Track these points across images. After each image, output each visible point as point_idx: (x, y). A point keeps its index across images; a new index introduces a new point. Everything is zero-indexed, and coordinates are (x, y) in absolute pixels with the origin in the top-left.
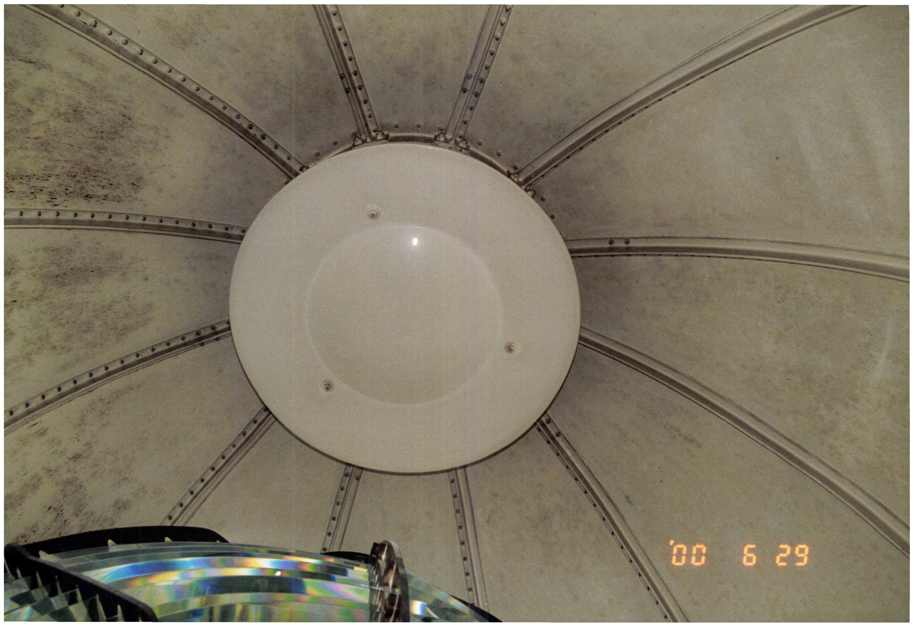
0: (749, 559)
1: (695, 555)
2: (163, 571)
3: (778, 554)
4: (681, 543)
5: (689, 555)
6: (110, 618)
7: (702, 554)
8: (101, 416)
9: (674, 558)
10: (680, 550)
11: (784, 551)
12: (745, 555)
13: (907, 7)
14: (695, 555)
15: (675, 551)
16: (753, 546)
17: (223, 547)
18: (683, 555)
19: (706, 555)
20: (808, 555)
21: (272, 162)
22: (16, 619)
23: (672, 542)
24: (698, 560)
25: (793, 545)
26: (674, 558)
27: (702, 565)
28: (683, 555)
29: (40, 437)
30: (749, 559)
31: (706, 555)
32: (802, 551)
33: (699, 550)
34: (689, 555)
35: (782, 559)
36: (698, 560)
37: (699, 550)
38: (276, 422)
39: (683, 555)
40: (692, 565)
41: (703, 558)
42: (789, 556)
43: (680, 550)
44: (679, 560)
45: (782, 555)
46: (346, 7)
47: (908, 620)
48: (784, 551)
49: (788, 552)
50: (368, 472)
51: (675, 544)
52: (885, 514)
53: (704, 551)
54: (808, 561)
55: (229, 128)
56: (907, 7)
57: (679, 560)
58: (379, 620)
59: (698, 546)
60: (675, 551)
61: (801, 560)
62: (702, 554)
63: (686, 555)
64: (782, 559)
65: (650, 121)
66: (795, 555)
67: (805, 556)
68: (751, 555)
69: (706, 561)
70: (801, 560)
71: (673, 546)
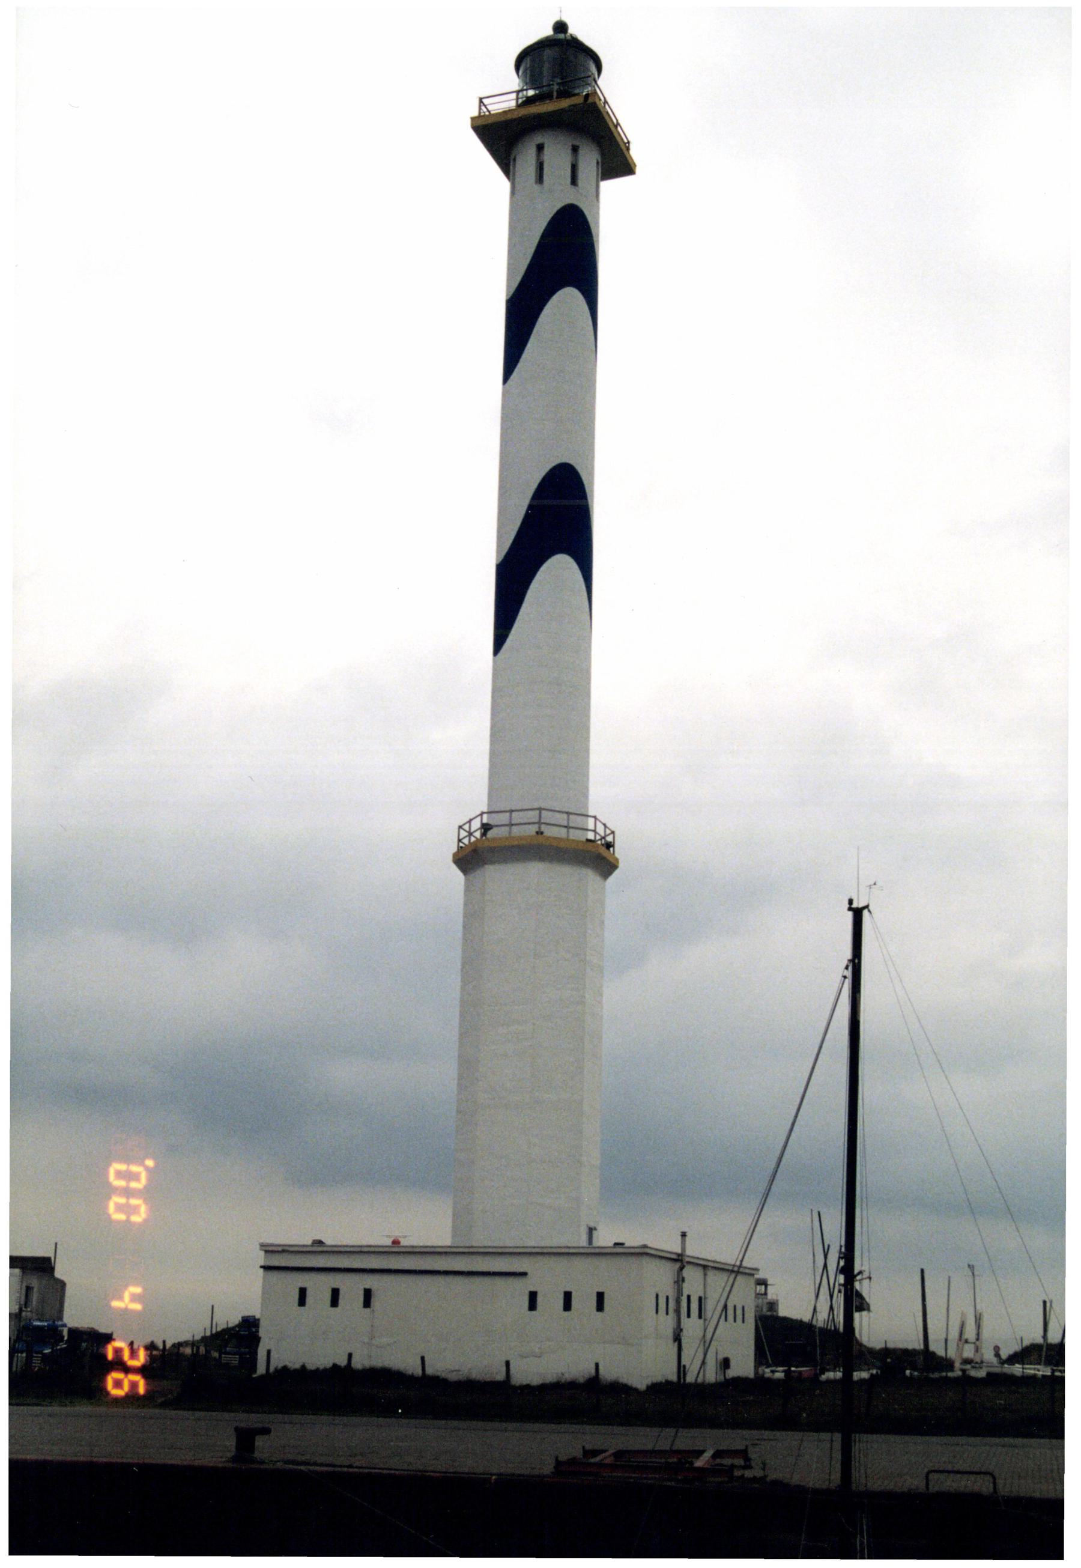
0: (118, 1384)
1: (127, 1202)
4: (148, 1179)
5: (128, 1192)
6: (13, 1317)
9: (122, 1167)
10: (136, 1177)
12: (126, 1376)
14: (127, 1202)
15: (134, 1168)
17: (293, 1464)
20: (126, 1309)
21: (663, 1251)
22: (12, 1266)
23: (150, 1163)
24: (119, 1208)
27: (109, 1216)
29: (558, 100)
33: (135, 1210)
34: (128, 1192)
36: (119, 1208)
37: (135, 1210)
41: (121, 1217)
43: (136, 1177)
44: (119, 1174)
51: (147, 1168)
54: (107, 1207)
55: (709, 1261)
57: (119, 1174)
59: (143, 1209)
60: (134, 1168)
61: (134, 1385)
63: (128, 1198)
68: (126, 1387)
69: (119, 1222)
70: (134, 1385)
71: (142, 1164)
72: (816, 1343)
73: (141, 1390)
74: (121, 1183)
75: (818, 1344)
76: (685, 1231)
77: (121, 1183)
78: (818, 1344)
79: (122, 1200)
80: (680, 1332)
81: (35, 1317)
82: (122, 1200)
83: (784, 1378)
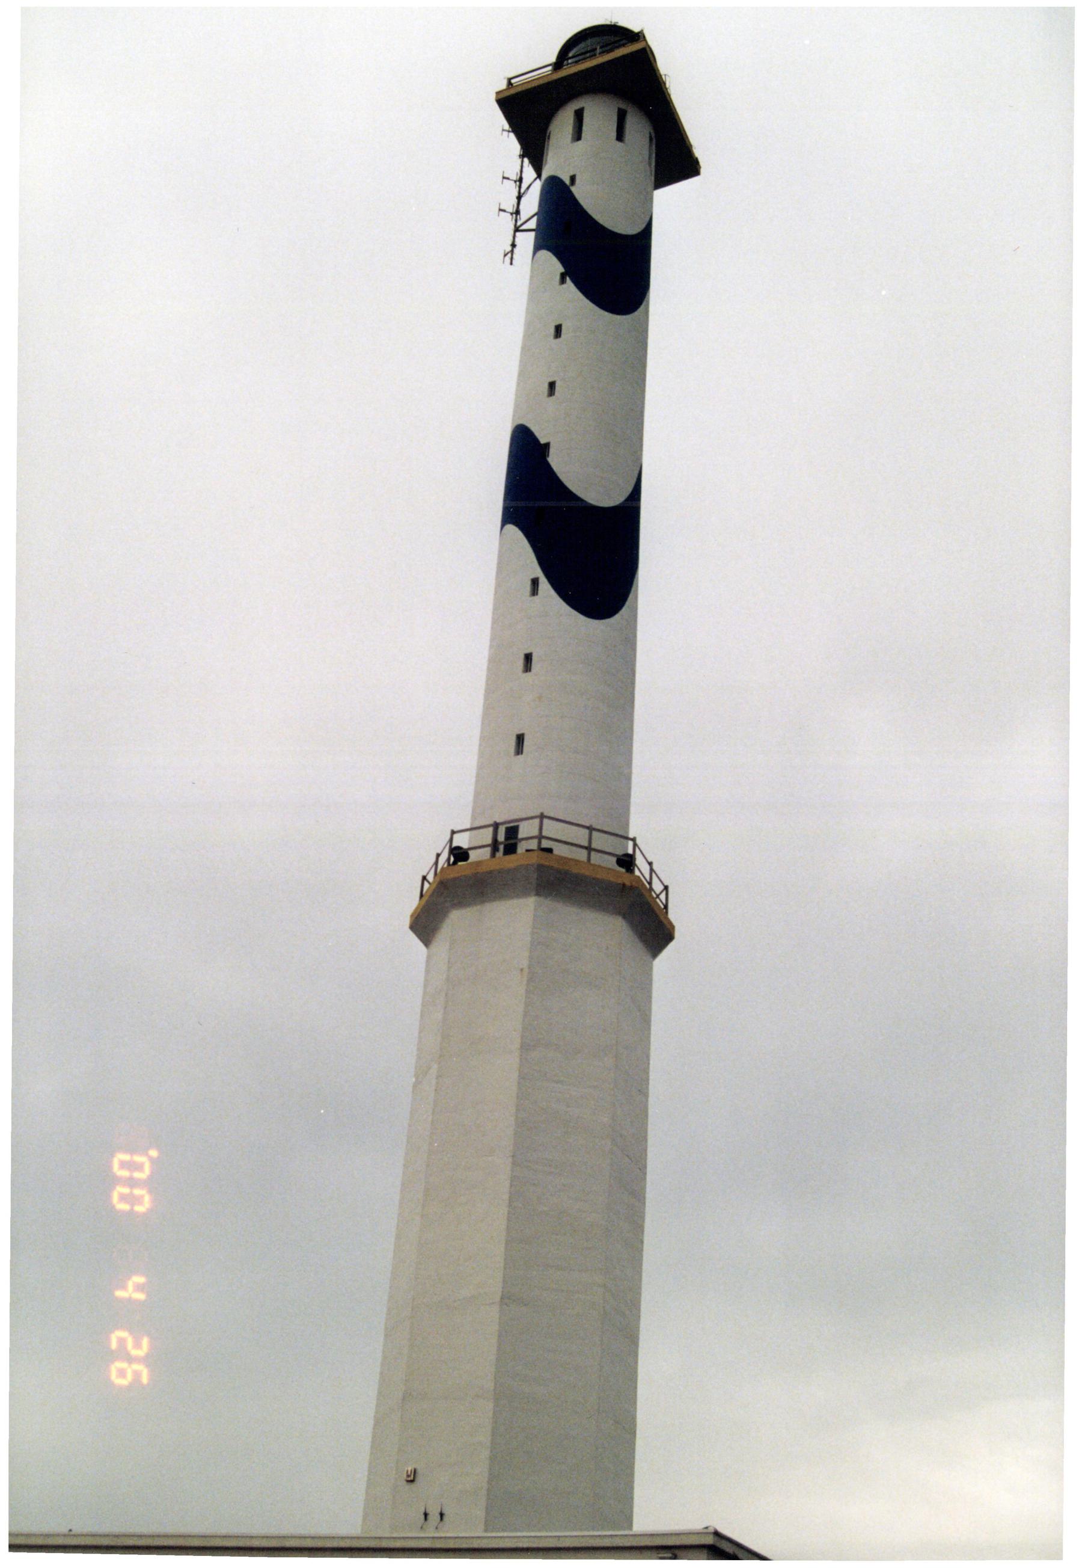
0: (122, 1373)
1: (131, 1192)
2: (671, 109)
3: (131, 1333)
7: (132, 1205)
9: (126, 1157)
10: (140, 1167)
11: (137, 1345)
15: (138, 1159)
16: (145, 1380)
18: (131, 1193)
20: (130, 1299)
24: (123, 1198)
25: (145, 1360)
26: (126, 1157)
27: (113, 1207)
32: (122, 1373)
35: (122, 1341)
36: (123, 1198)
37: (139, 1200)
38: (594, 833)
40: (115, 1188)
41: (124, 1207)
43: (140, 1167)
44: (123, 1165)
46: (635, 552)
48: (137, 1345)
49: (135, 1352)
51: (151, 1159)
53: (139, 1209)
54: (110, 1197)
57: (123, 1165)
59: (147, 1198)
60: (138, 1159)
61: (137, 1375)
62: (132, 1205)
64: (122, 1341)
65: (553, 879)
68: (130, 1376)
69: (123, 1212)
71: (147, 1155)
73: (145, 1380)
74: (125, 1173)
77: (125, 1173)
79: (126, 1190)
82: (126, 1190)
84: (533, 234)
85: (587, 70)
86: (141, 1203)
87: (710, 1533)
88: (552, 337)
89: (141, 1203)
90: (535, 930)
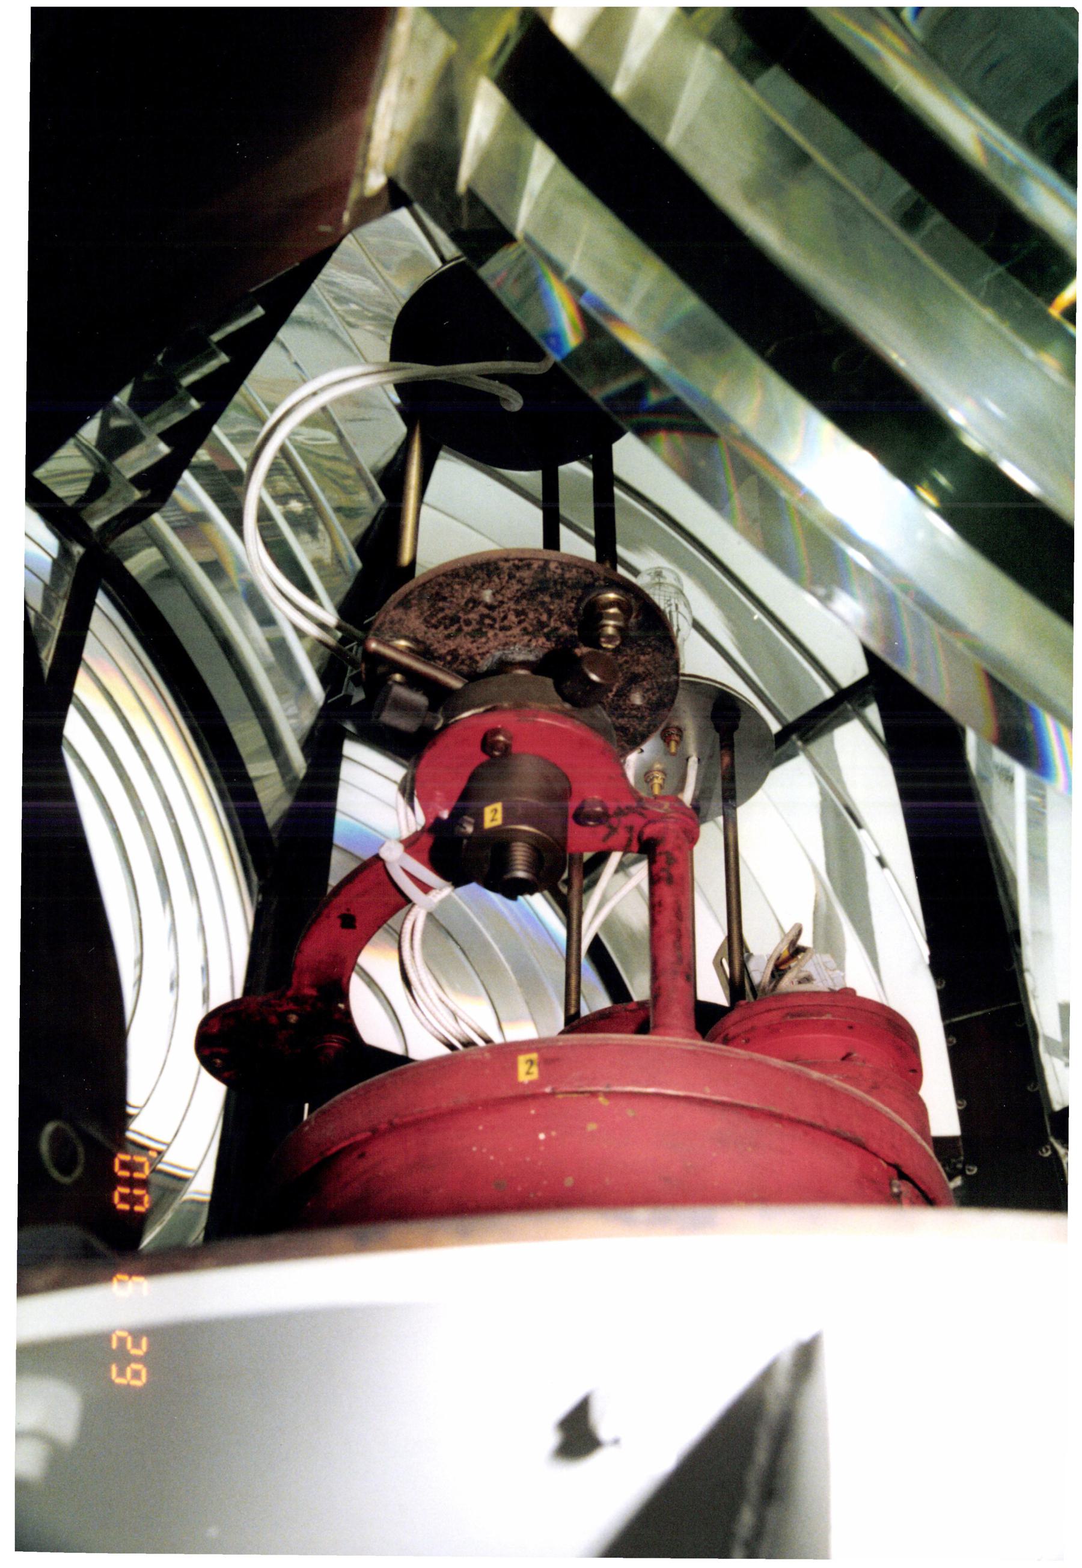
7: (132, 1205)
8: (681, 325)
13: (17, 1549)
19: (132, 1211)
20: (128, 1385)
24: (123, 1198)
27: (114, 1206)
28: (131, 1194)
30: (136, 1375)
31: (132, 1211)
32: (136, 1375)
36: (123, 1198)
37: (139, 1200)
39: (131, 1194)
41: (125, 1207)
42: (128, 1352)
45: (129, 1345)
47: (32, 8)
49: (135, 1352)
50: (255, 721)
52: (125, 635)
54: (111, 1198)
56: (17, 1549)
58: (69, 804)
61: (122, 1373)
62: (132, 1205)
63: (131, 1177)
66: (129, 1364)
67: (127, 1380)
69: (123, 1211)
70: (122, 1373)
72: (997, 1011)
73: (114, 1369)
74: (125, 1174)
75: (998, 1008)
76: (345, 932)
77: (125, 1174)
78: (998, 1008)
79: (126, 1191)
80: (699, 798)
81: (115, 423)
82: (126, 1191)
83: (444, 446)
84: (328, 651)
85: (378, 1074)
86: (141, 1203)
87: (565, 828)
88: (355, 931)
89: (141, 1203)
90: (263, 524)
